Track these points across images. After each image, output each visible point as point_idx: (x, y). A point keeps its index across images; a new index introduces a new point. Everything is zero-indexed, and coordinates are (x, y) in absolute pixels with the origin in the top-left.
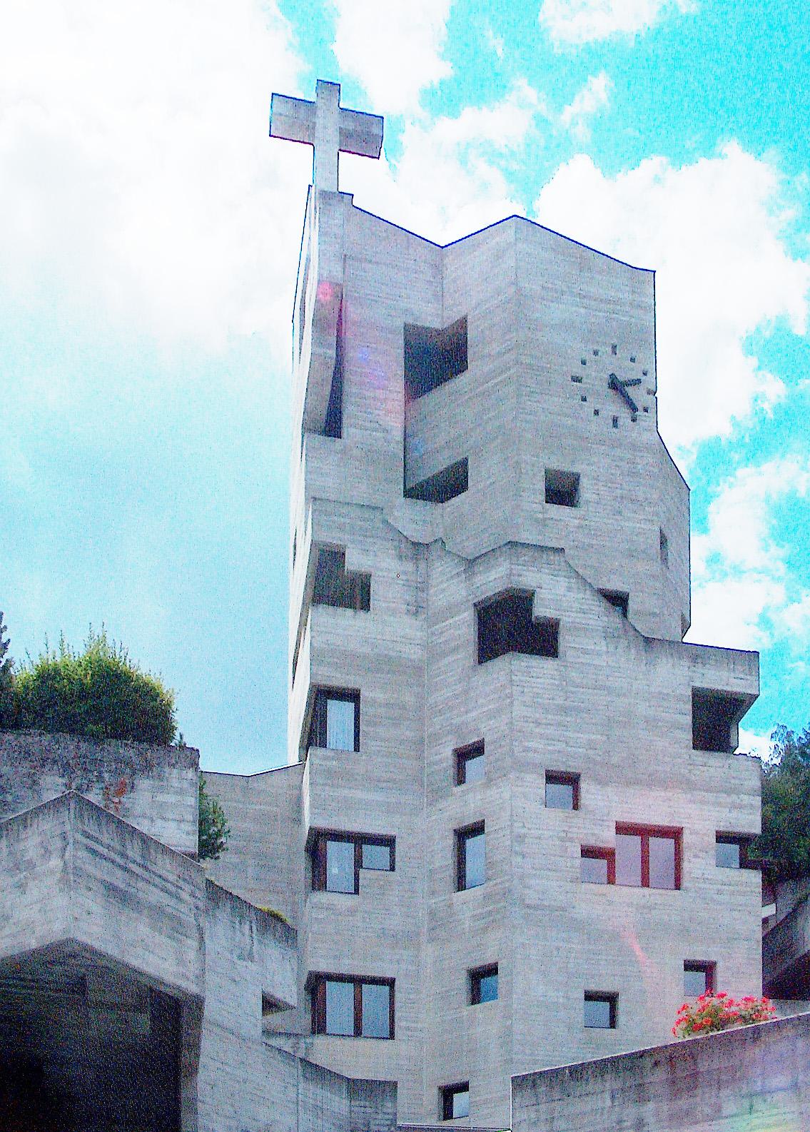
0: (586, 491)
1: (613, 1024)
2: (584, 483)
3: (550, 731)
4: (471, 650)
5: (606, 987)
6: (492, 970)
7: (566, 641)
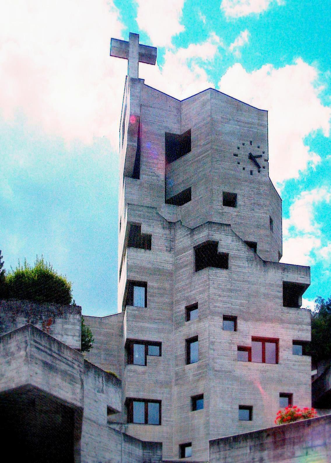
0: (240, 201)
1: (250, 419)
2: (239, 197)
3: (225, 299)
5: (247, 403)
6: (201, 397)
7: (231, 262)
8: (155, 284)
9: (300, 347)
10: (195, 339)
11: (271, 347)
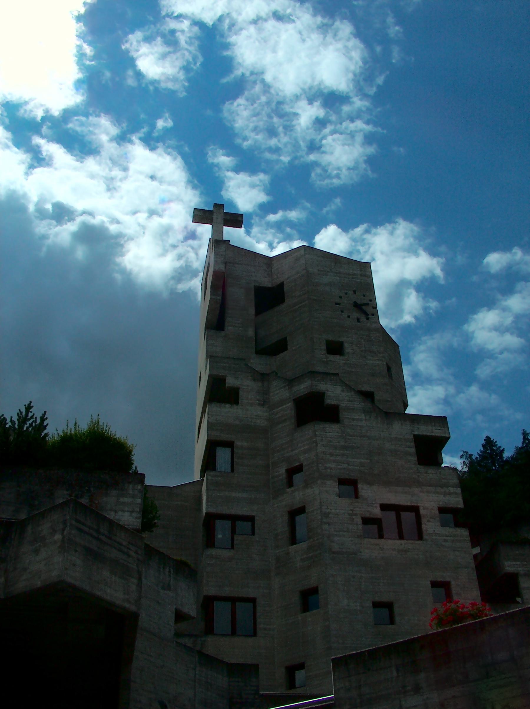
0: (348, 349)
1: (392, 621)
2: (346, 345)
3: (338, 458)
5: (385, 598)
6: (314, 591)
7: (344, 415)
8: (245, 444)
9: (450, 517)
10: (302, 510)
11: (408, 517)
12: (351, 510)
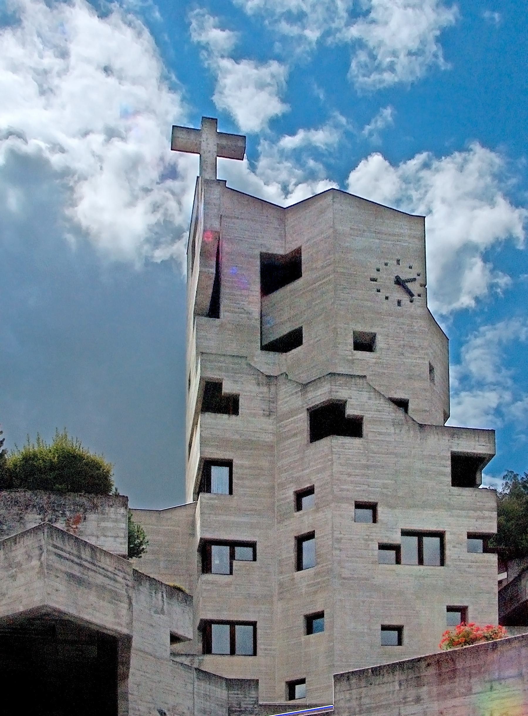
0: (380, 343)
2: (379, 338)
3: (358, 479)
4: (306, 435)
6: (320, 615)
7: (366, 428)
8: (246, 463)
12: (367, 535)
